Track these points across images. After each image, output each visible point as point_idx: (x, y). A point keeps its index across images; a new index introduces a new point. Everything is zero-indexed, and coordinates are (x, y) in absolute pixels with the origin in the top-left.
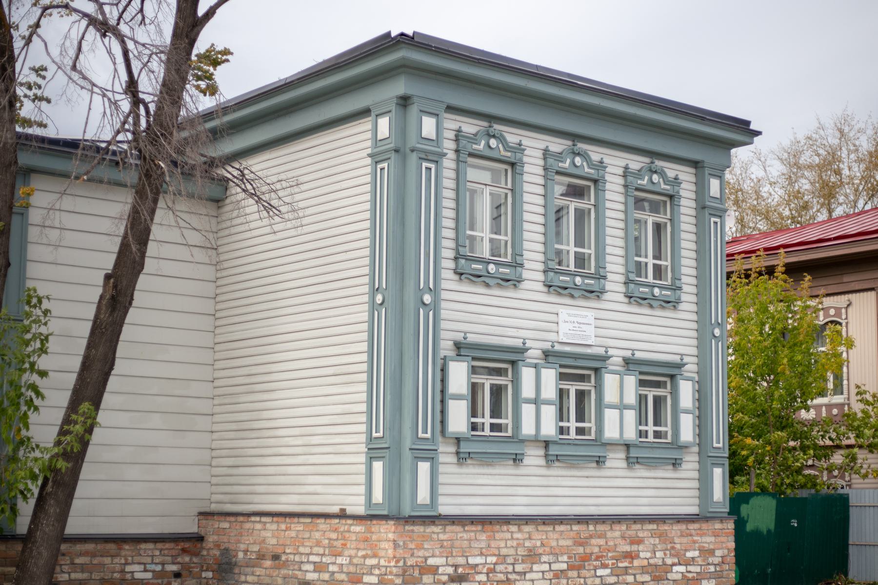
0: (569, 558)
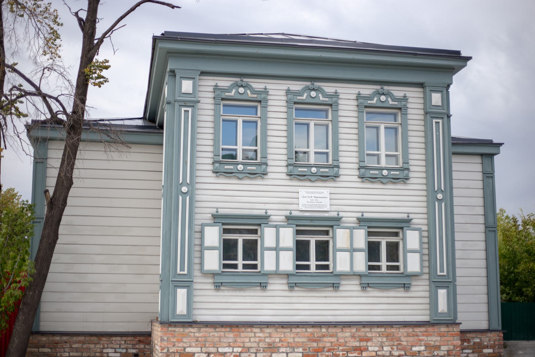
0: (304, 350)
